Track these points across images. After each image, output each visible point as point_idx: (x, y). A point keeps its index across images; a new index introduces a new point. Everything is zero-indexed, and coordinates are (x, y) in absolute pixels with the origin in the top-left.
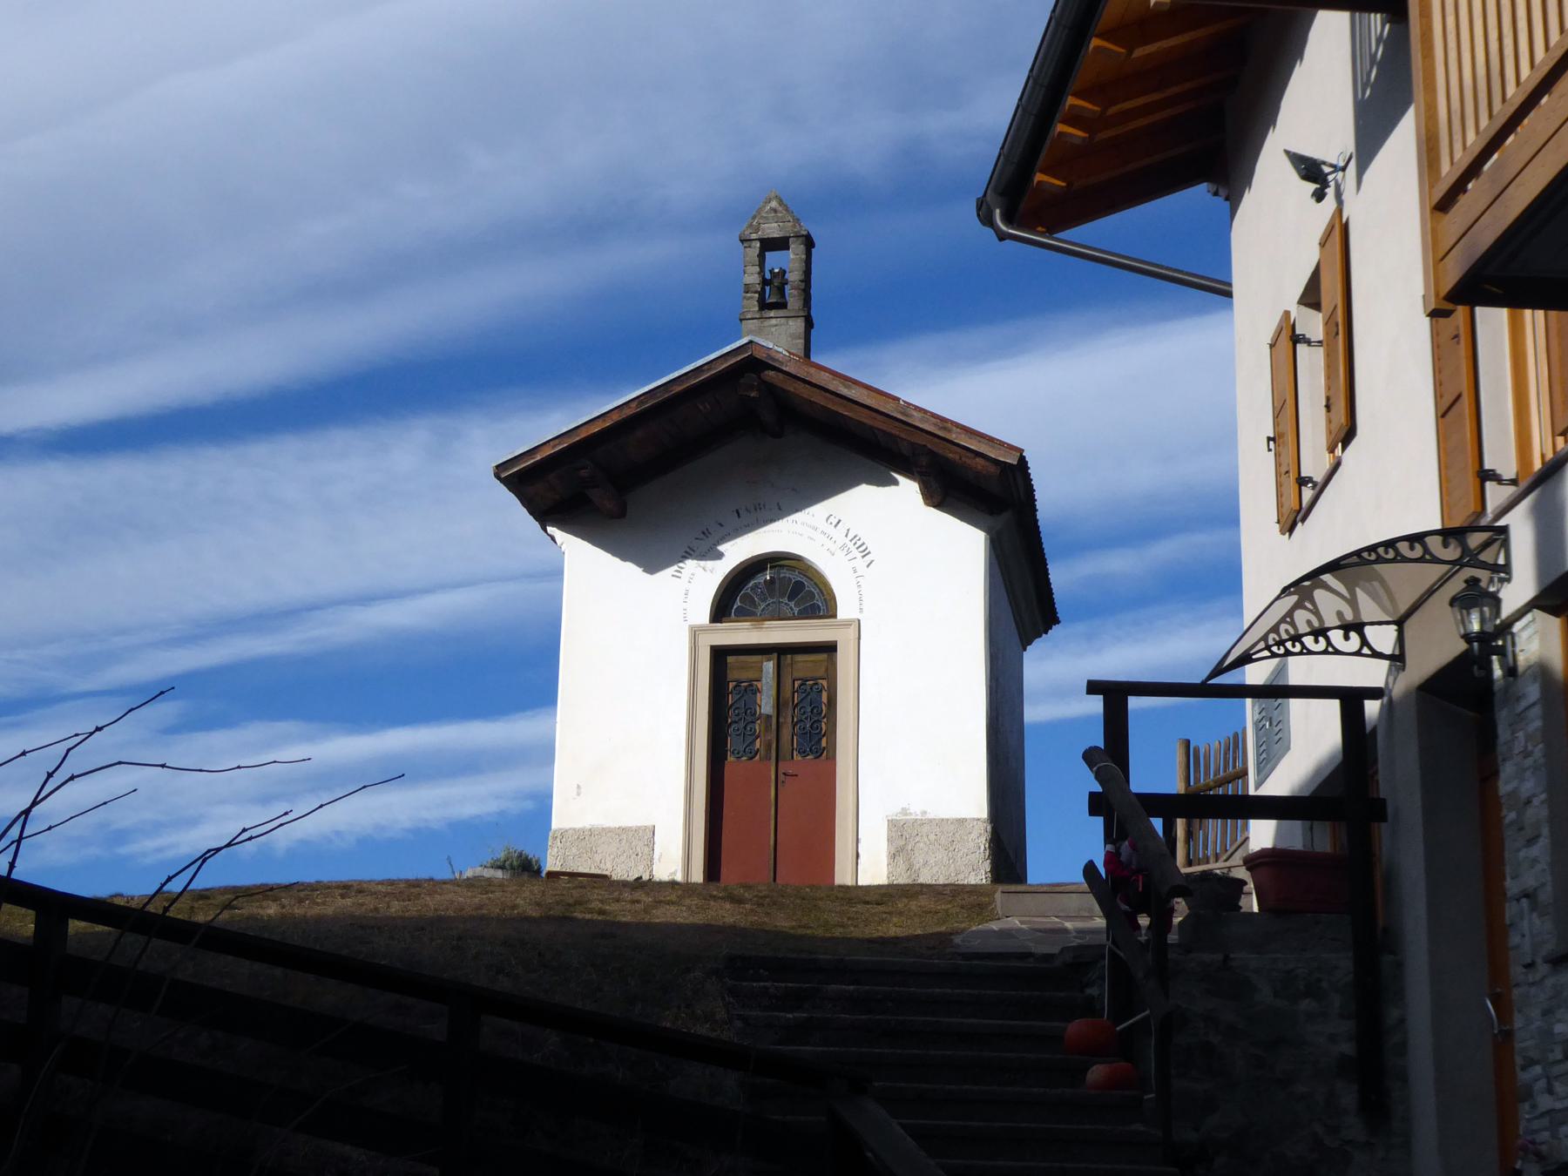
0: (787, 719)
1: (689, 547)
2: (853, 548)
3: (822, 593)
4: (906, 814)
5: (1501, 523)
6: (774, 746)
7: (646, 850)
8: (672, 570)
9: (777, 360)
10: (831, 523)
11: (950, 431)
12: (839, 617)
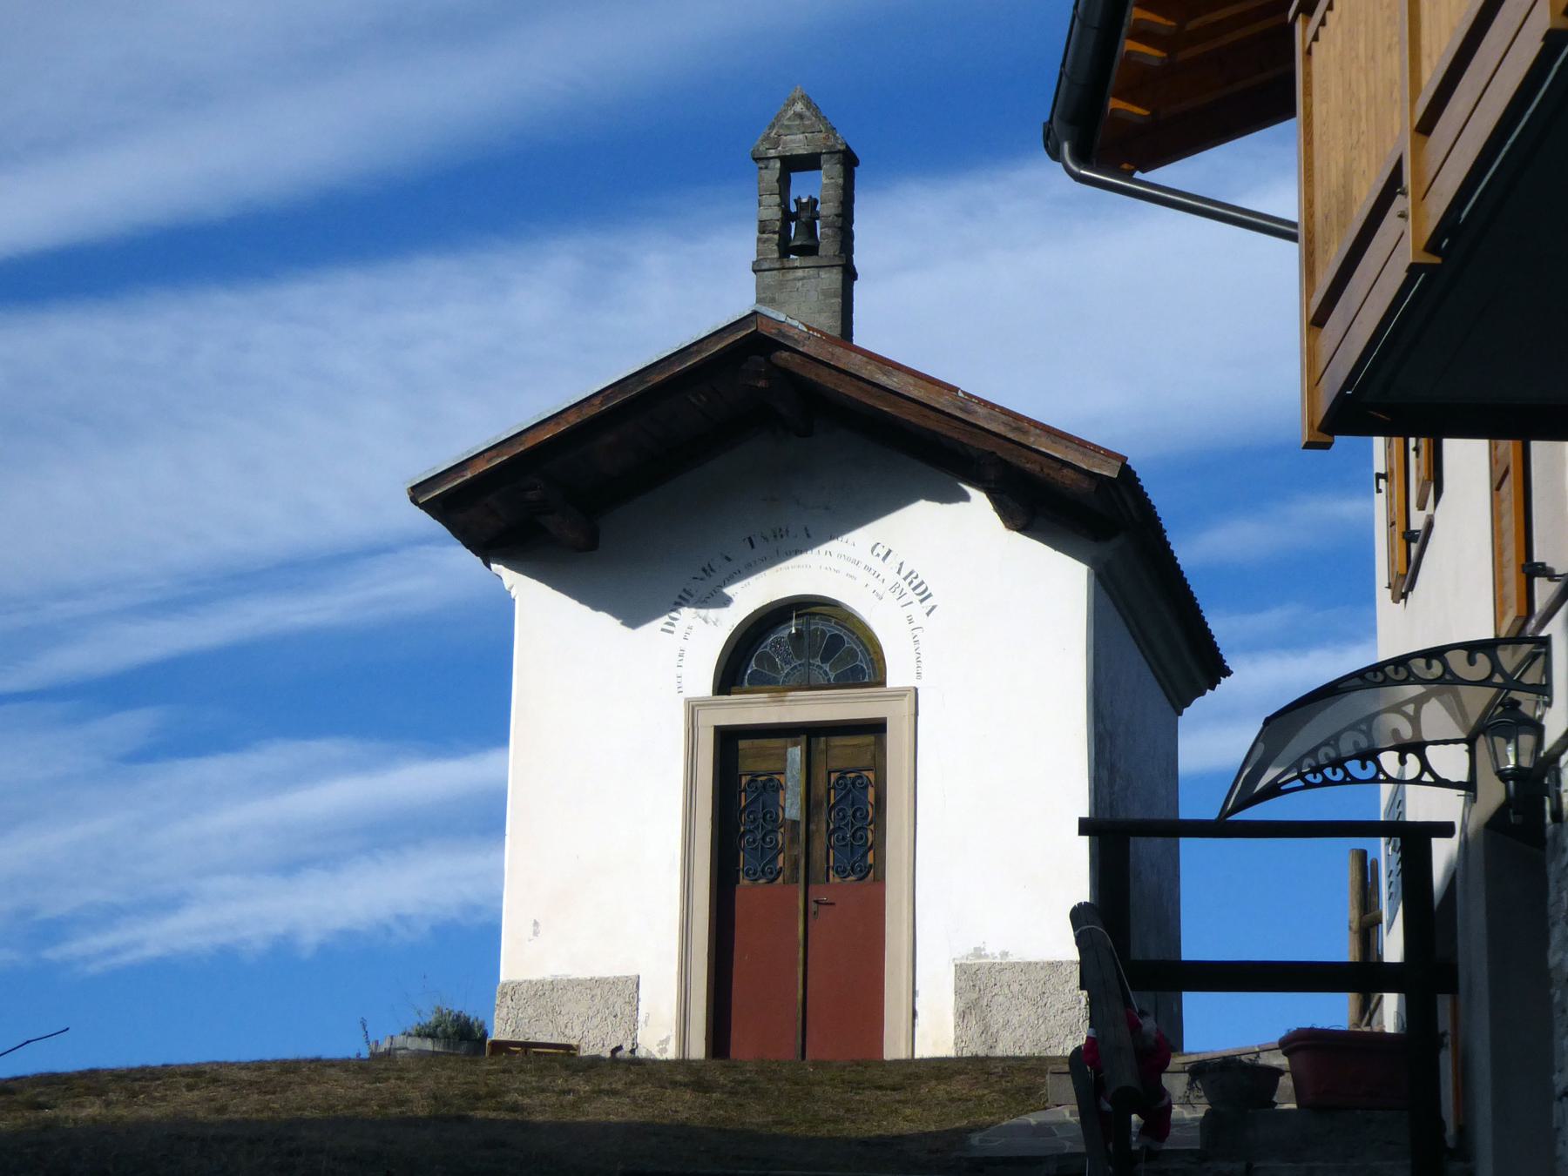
0: (821, 827)
1: (685, 590)
2: (908, 589)
3: (867, 650)
4: (980, 956)
5: (1543, 634)
7: (628, 1009)
8: (661, 622)
11: (1025, 433)
12: (888, 685)
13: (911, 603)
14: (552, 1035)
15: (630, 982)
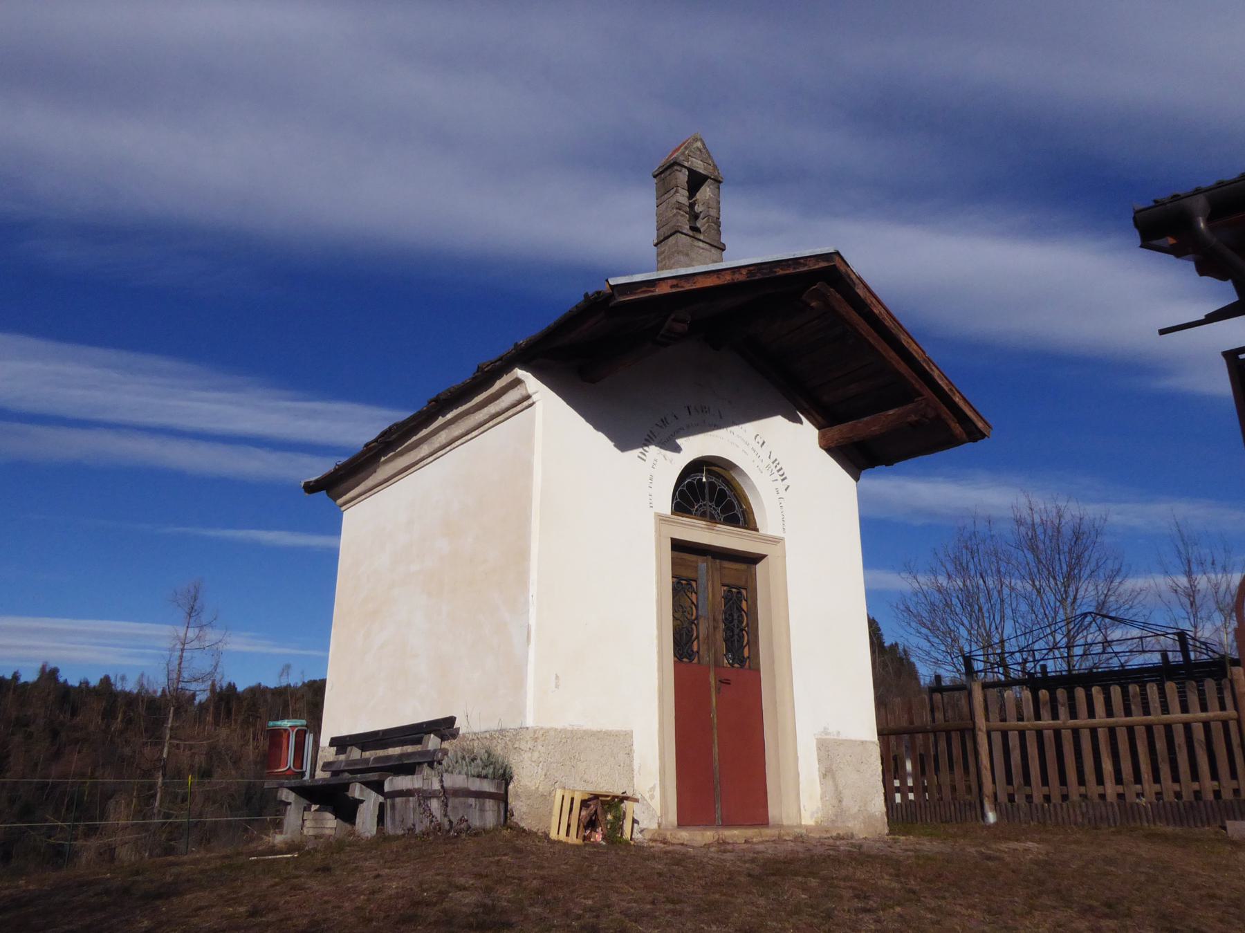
1: (651, 431)
4: (826, 734)
8: (637, 452)
11: (954, 394)
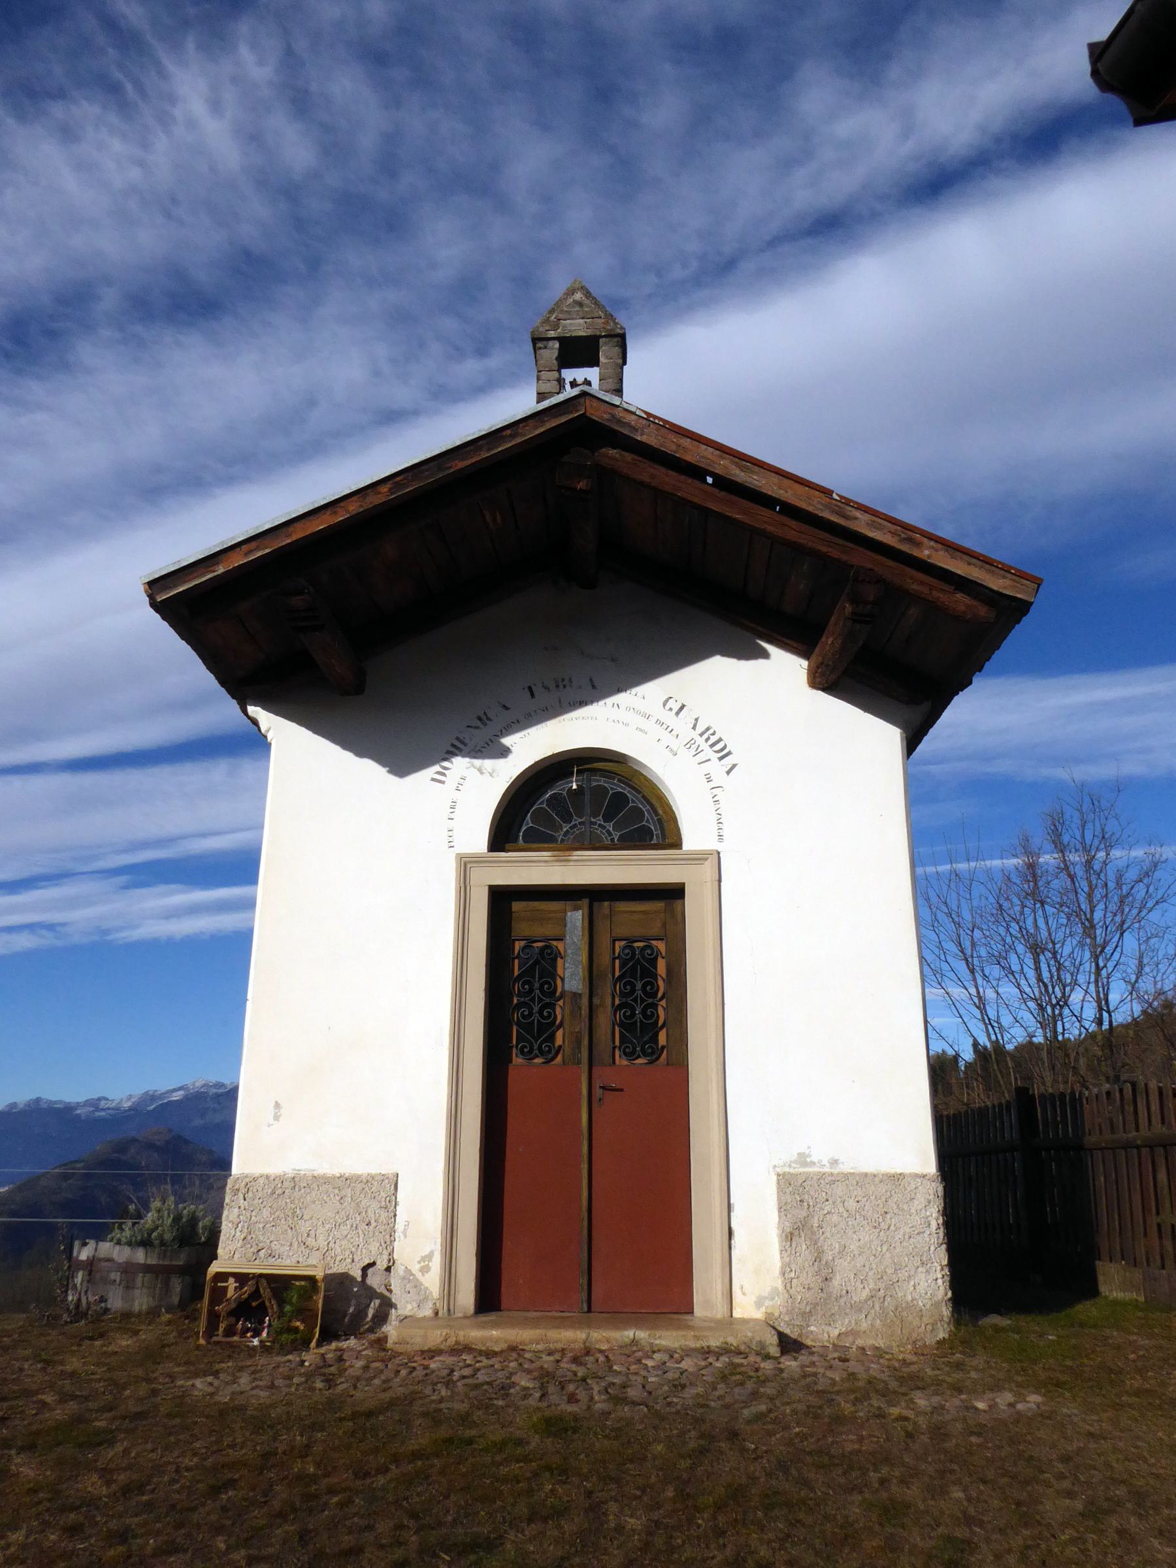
1: (457, 738)
2: (705, 746)
6: (586, 1042)
7: (384, 1215)
8: (431, 771)
9: (628, 425)
10: (671, 709)
11: (918, 545)
13: (709, 760)
14: (291, 1245)
15: (387, 1181)
